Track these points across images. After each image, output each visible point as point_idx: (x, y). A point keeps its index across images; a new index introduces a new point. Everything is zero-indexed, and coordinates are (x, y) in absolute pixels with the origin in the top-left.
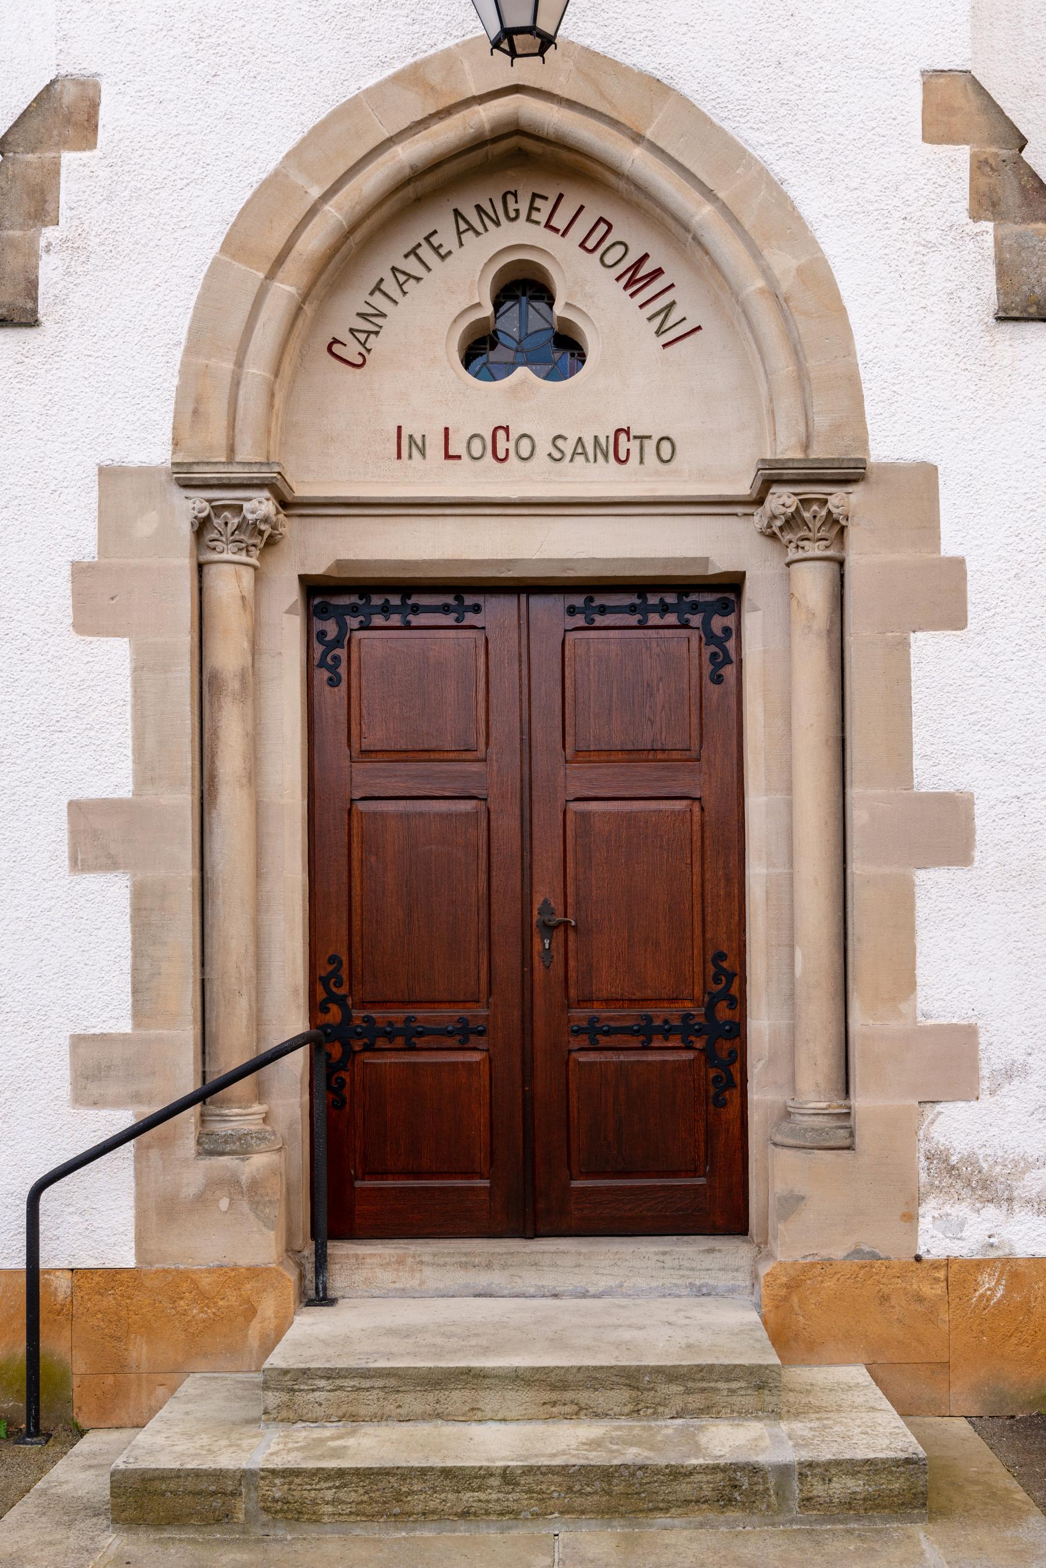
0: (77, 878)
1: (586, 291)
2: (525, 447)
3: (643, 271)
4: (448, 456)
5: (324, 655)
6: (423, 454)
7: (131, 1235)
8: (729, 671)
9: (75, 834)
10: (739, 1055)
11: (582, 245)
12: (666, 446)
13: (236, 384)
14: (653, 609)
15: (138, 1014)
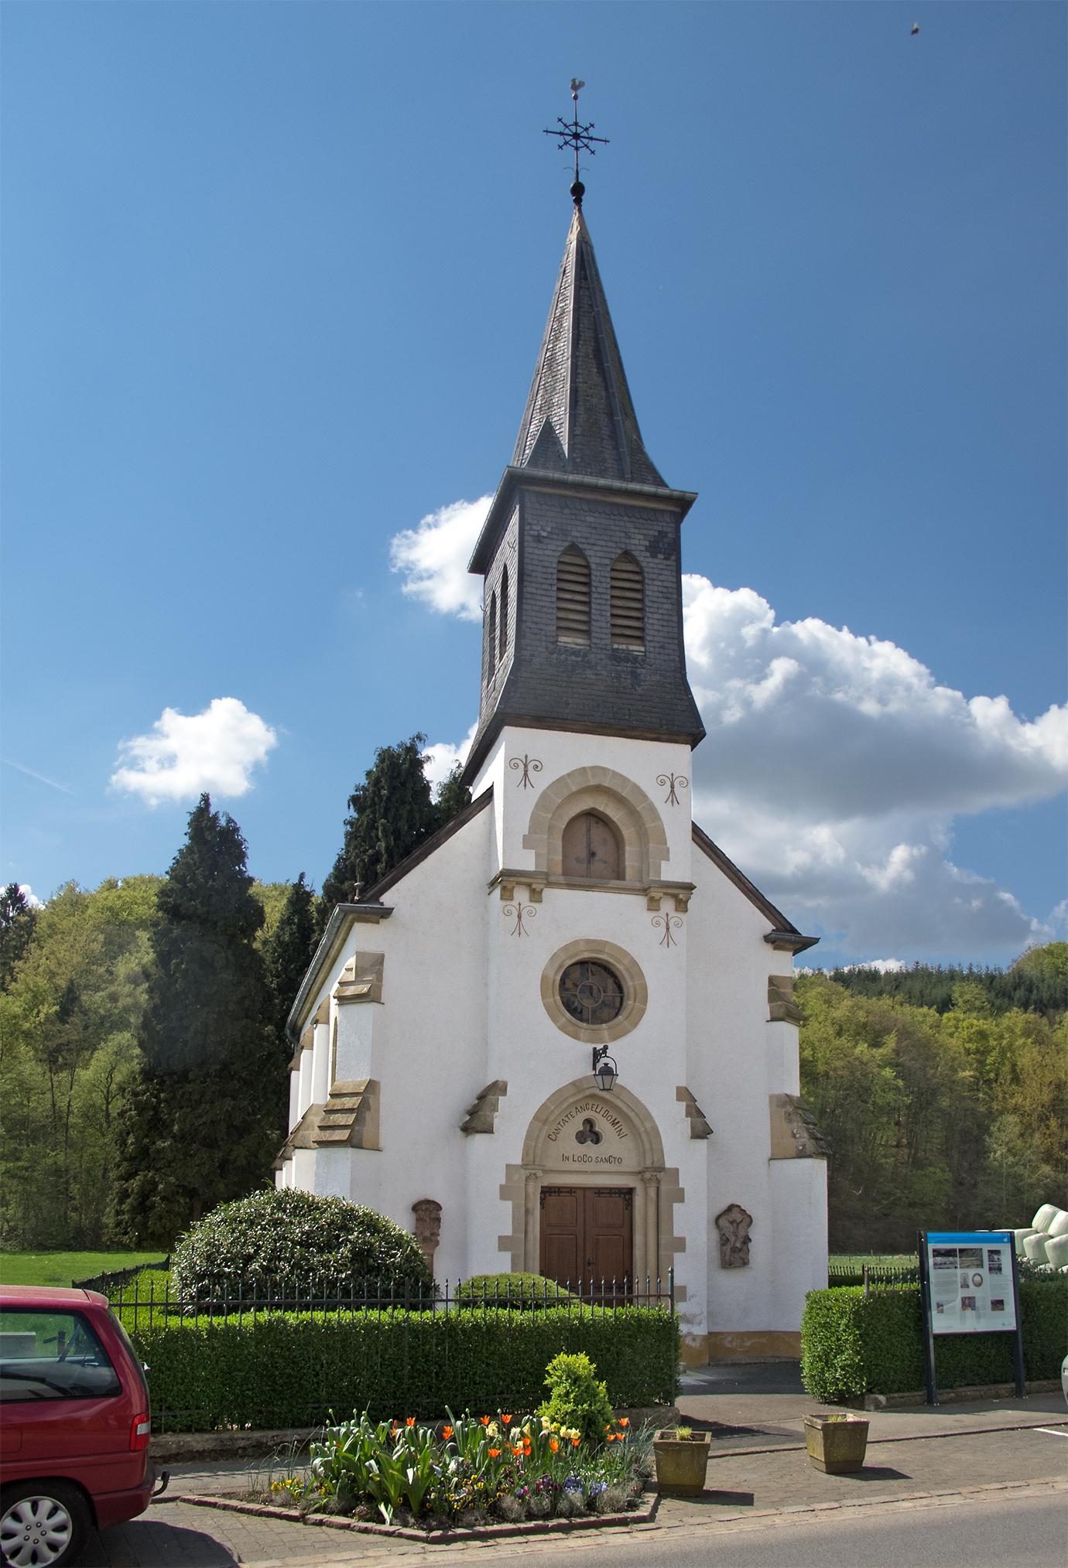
1: (603, 1125)
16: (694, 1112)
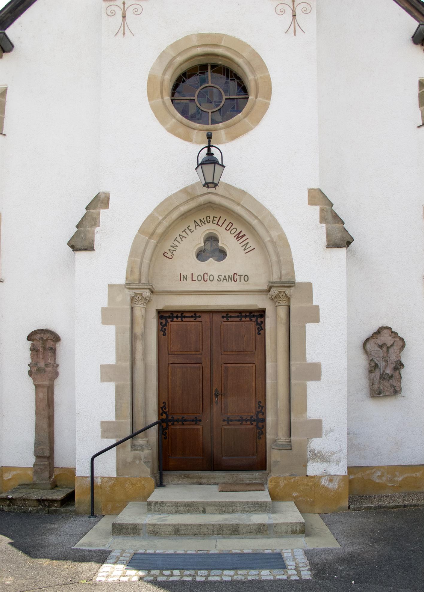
0: (102, 383)
1: (227, 240)
2: (211, 278)
3: (241, 235)
4: (192, 280)
5: (162, 328)
6: (186, 280)
7: (115, 469)
8: (262, 332)
9: (102, 372)
10: (264, 427)
11: (226, 229)
12: (246, 277)
13: (141, 264)
14: (243, 317)
15: (117, 416)
16: (331, 217)
